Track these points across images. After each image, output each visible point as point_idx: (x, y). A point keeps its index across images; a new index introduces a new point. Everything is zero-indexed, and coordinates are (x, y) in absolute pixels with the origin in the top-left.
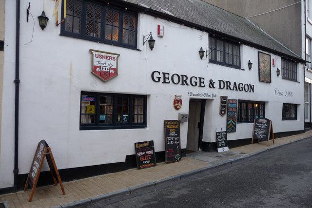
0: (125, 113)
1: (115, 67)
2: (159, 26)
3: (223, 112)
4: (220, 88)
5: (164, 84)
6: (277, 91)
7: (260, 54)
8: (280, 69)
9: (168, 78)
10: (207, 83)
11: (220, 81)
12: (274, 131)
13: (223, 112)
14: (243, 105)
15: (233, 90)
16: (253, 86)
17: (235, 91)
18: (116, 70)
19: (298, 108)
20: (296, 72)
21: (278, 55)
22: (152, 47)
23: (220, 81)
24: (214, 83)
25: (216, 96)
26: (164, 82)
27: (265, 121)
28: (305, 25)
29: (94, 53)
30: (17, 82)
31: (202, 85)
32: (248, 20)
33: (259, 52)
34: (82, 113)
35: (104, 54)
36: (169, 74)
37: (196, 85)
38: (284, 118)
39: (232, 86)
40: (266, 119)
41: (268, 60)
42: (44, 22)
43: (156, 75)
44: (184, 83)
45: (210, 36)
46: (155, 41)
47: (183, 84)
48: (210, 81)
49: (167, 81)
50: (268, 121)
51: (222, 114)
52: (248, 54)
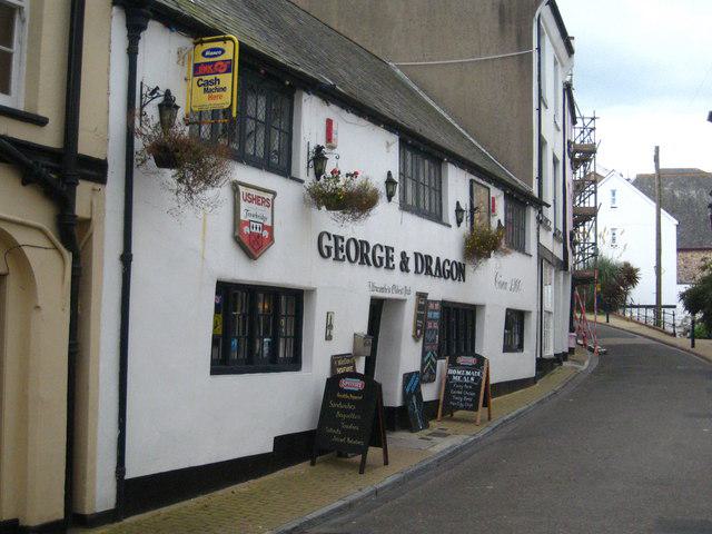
0: (266, 335)
1: (268, 223)
2: (329, 123)
6: (499, 279)
7: (475, 186)
8: (396, 177)
18: (271, 229)
19: (6, 165)
20: (440, 191)
21: (369, 120)
26: (336, 259)
27: (471, 361)
28: (539, 109)
29: (242, 189)
30: (126, 259)
31: (391, 265)
32: (398, 71)
33: (471, 181)
35: (254, 193)
37: (329, 255)
38: (507, 348)
39: (433, 267)
40: (475, 356)
41: (487, 202)
43: (326, 242)
45: (403, 144)
47: (362, 263)
50: (481, 361)
51: (416, 338)
52: (457, 186)
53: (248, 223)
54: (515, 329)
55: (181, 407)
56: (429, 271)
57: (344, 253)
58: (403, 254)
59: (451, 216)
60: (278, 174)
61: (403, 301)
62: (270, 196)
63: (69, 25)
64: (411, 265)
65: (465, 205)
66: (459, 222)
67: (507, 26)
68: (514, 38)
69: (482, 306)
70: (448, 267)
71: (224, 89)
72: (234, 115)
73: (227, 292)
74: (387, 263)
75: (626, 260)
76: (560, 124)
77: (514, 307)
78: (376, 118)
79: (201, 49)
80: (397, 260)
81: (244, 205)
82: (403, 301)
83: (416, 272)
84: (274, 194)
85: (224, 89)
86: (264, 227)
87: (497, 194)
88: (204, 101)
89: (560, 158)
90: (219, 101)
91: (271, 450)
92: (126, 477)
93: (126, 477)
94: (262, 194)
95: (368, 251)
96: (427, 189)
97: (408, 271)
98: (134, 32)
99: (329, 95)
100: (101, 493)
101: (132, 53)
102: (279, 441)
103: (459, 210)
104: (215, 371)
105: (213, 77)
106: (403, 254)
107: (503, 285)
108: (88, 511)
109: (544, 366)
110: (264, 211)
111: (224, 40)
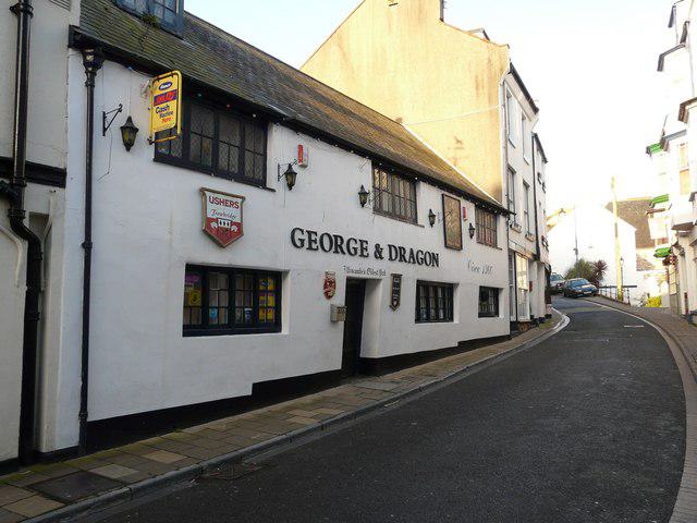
1: (238, 220)
2: (301, 147)
18: (239, 225)
26: (310, 248)
31: (365, 254)
39: (407, 256)
43: (298, 235)
45: (374, 165)
53: (216, 220)
54: (491, 300)
55: (147, 359)
56: (402, 258)
57: (318, 244)
58: (377, 246)
59: (423, 218)
60: (223, 178)
61: (379, 280)
62: (239, 200)
63: (463, 189)
64: (385, 254)
65: (437, 210)
66: (432, 224)
67: (481, 91)
68: (486, 100)
69: (287, 272)
70: (421, 256)
71: (172, 113)
72: (178, 132)
73: (198, 275)
74: (362, 250)
75: (601, 259)
76: (530, 161)
77: (486, 285)
78: (346, 146)
79: (158, 84)
80: (371, 250)
81: (210, 207)
82: (379, 280)
83: (391, 259)
84: (243, 198)
85: (172, 113)
86: (233, 223)
87: (470, 209)
88: (160, 124)
89: (530, 183)
90: (168, 123)
91: (250, 393)
92: (88, 420)
93: (88, 420)
94: (220, 196)
95: (342, 243)
96: (402, 195)
97: (382, 258)
98: (92, 69)
99: (297, 126)
100: (60, 430)
101: (90, 85)
102: (256, 386)
103: (432, 216)
104: (189, 331)
105: (164, 105)
106: (377, 246)
107: (476, 269)
108: (44, 449)
109: (515, 325)
110: (234, 212)
111: (172, 75)
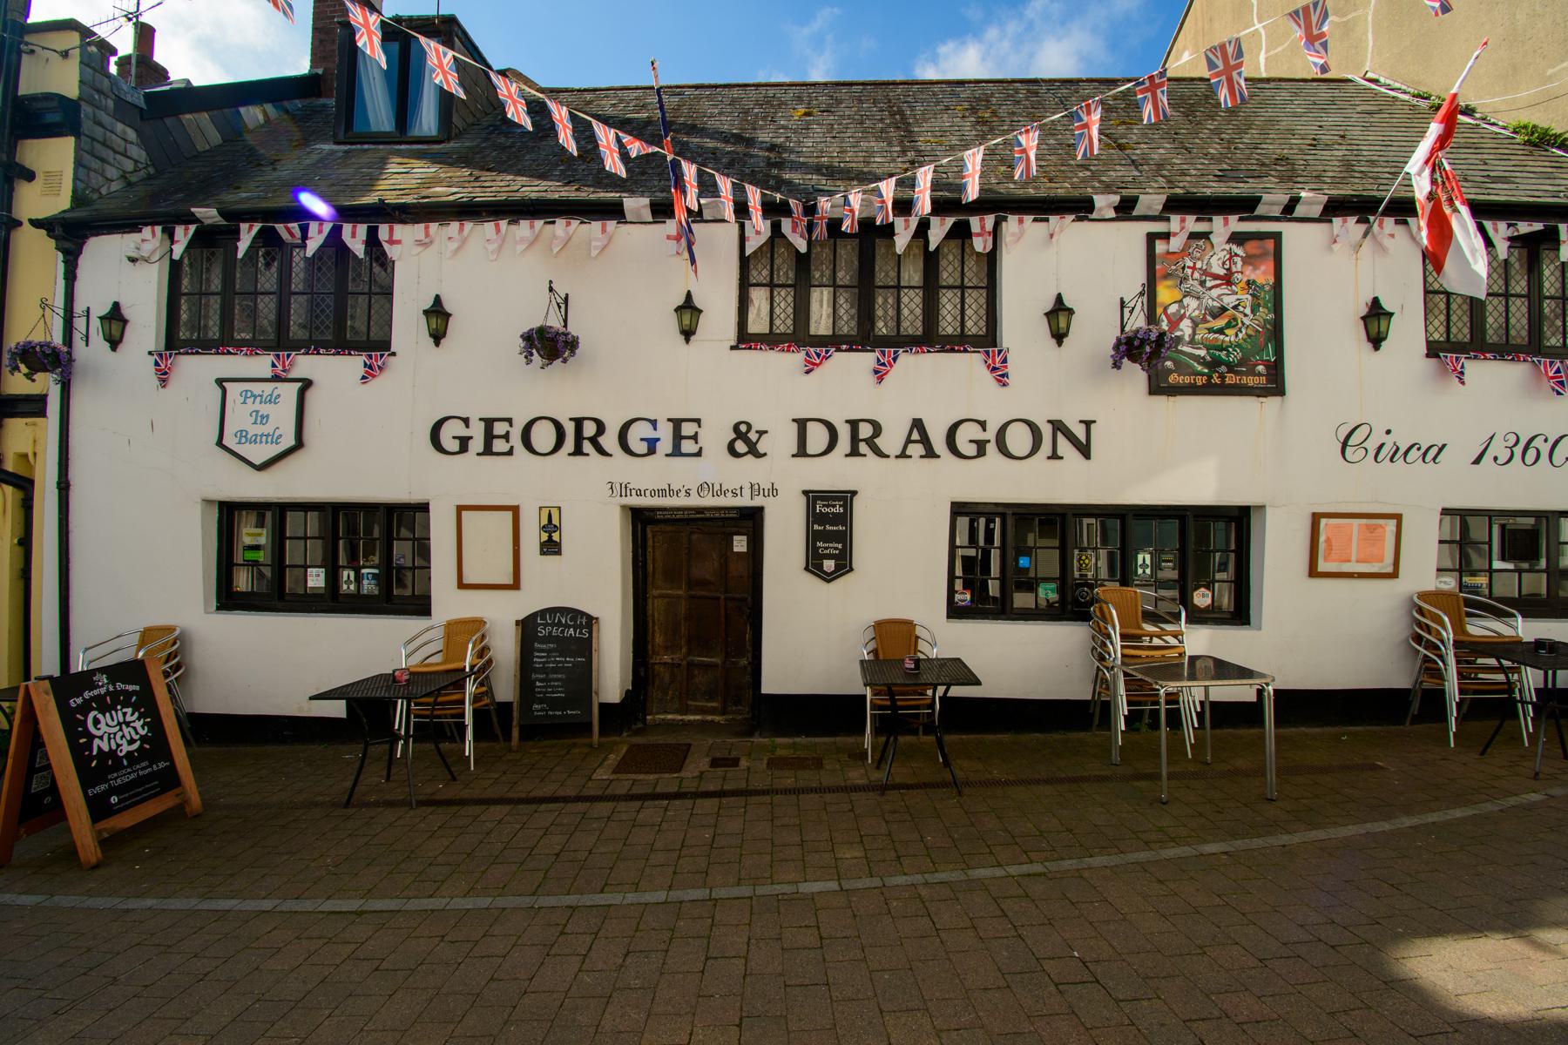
3: (829, 565)
4: (802, 452)
5: (488, 460)
9: (506, 437)
10: (715, 436)
11: (802, 424)
12: (775, 681)
13: (829, 565)
14: (251, 534)
15: (903, 455)
16: (1088, 424)
17: (917, 464)
22: (438, 337)
23: (802, 424)
24: (761, 433)
25: (773, 491)
26: (488, 451)
34: (958, 543)
36: (510, 421)
42: (116, 327)
44: (863, 448)
46: (1391, 315)
48: (736, 428)
49: (499, 446)
